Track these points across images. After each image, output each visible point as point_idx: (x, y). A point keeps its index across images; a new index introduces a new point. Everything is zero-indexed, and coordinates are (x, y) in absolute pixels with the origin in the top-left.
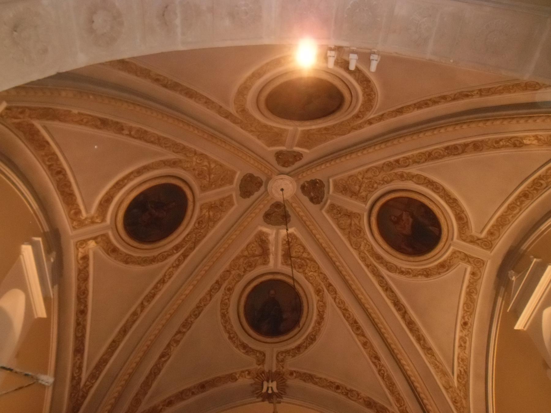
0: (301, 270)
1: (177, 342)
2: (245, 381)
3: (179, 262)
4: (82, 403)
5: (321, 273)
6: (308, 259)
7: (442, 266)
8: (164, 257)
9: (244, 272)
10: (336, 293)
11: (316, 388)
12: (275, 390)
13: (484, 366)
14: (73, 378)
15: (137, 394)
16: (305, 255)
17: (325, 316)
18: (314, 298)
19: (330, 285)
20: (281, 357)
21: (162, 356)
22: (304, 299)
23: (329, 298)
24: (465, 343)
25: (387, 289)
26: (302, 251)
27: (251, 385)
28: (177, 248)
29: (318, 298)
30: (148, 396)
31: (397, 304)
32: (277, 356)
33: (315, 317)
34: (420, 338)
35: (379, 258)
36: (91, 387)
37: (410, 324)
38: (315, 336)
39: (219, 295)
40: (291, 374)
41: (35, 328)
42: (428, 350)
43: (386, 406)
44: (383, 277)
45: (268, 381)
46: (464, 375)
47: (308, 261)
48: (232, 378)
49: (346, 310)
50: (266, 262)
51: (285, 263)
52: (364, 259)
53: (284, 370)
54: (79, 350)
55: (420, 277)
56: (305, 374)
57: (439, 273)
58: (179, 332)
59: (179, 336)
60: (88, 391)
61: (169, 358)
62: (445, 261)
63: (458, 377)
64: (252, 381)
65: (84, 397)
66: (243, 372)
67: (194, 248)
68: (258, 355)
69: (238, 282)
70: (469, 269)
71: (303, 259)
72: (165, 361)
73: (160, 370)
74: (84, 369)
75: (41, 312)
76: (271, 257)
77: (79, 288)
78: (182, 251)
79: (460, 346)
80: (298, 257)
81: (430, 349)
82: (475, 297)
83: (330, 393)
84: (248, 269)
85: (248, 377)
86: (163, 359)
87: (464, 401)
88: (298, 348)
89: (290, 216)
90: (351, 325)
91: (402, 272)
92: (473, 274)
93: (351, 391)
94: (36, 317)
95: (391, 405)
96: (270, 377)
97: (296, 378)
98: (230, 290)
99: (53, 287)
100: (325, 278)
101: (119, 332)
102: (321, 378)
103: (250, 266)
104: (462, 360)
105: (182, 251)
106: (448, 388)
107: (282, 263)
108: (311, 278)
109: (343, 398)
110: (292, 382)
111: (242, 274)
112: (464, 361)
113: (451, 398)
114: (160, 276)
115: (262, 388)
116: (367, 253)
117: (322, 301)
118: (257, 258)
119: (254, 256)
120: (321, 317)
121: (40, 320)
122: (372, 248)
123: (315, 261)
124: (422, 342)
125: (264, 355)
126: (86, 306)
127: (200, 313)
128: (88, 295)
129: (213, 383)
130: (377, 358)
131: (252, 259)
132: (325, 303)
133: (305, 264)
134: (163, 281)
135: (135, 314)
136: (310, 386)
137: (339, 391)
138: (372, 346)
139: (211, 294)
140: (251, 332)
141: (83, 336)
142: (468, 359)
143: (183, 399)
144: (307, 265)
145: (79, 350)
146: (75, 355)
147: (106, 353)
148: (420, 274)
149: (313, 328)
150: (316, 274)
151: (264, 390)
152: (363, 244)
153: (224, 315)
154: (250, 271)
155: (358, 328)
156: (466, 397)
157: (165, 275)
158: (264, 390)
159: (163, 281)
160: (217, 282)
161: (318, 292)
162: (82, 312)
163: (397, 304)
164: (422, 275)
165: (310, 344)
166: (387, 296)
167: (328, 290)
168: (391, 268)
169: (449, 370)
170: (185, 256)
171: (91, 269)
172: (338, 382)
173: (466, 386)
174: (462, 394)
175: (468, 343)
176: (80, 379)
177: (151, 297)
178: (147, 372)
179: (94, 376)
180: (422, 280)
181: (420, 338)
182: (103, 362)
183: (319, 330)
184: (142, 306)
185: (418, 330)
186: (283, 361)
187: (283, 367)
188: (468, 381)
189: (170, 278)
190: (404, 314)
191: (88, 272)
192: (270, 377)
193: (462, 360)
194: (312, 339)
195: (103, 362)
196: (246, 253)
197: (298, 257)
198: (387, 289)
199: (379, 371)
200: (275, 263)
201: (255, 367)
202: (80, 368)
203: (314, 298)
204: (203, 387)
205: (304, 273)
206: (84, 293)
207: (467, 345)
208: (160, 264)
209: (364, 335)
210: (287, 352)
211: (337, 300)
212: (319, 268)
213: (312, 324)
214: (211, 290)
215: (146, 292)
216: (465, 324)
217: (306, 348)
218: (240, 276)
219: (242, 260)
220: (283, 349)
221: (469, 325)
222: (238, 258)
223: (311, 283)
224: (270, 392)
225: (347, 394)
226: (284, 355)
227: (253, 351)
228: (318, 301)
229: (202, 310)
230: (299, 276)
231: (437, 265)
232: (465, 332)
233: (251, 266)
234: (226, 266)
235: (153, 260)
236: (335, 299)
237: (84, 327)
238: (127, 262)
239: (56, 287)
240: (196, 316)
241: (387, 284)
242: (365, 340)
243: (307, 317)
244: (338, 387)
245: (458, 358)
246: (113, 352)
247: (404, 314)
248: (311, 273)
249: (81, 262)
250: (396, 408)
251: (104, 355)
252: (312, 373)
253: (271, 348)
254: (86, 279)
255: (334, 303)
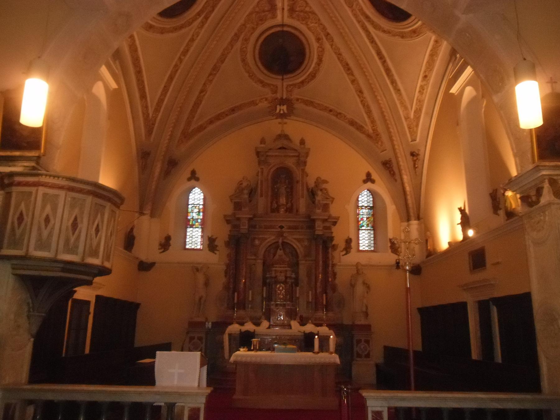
0: (304, 22)
1: (211, 81)
2: (264, 105)
3: (203, 23)
4: (153, 128)
5: (321, 24)
6: (310, 12)
7: (414, 31)
8: (190, 23)
9: (257, 25)
10: (333, 41)
11: (316, 110)
12: (286, 111)
13: (432, 109)
14: (143, 114)
15: (188, 118)
16: (307, 9)
17: (323, 59)
18: (315, 45)
19: (328, 34)
20: (290, 89)
21: (202, 91)
22: (307, 46)
23: (327, 46)
24: (423, 90)
25: (372, 41)
26: (305, 5)
27: (269, 107)
28: (199, 14)
29: (318, 45)
30: (195, 119)
31: (379, 53)
32: (287, 88)
33: (315, 60)
34: (393, 82)
35: (367, 17)
36: (157, 117)
37: (388, 71)
38: (315, 74)
39: (238, 45)
40: (298, 100)
41: (113, 95)
42: (398, 90)
43: (363, 125)
44: (370, 33)
45: (280, 105)
46: (418, 112)
47: (310, 14)
48: (253, 103)
49: (340, 54)
50: (274, 16)
51: (291, 16)
52: (355, 15)
53: (292, 97)
54: (143, 96)
55: (397, 37)
56: (307, 100)
57: (411, 37)
58: (210, 74)
59: (211, 78)
60: (155, 120)
61: (206, 93)
62: (416, 29)
63: (415, 112)
64: (269, 105)
65: (154, 124)
66: (262, 99)
67: (213, 10)
68: (272, 87)
69: (252, 33)
70: (434, 38)
71: (306, 12)
72: (204, 95)
73: (201, 101)
74: (150, 108)
75: (113, 85)
76: (279, 13)
77: (132, 57)
78: (203, 16)
79: (420, 92)
80: (302, 11)
81: (399, 90)
82: (436, 58)
83: (326, 114)
84: (260, 22)
85: (266, 102)
86: (202, 94)
87: (415, 129)
88: (302, 82)
89: (209, 250)
90: (343, 66)
91: (384, 31)
92: (436, 41)
93: (340, 113)
94: (112, 89)
95: (366, 125)
96: (282, 102)
97: (300, 103)
98: (246, 40)
99: (115, 63)
100: (324, 29)
101: (168, 80)
102: (319, 104)
103: (261, 20)
104: (420, 101)
105: (203, 16)
106: (407, 118)
107: (288, 17)
108: (312, 29)
109: (334, 118)
110: (299, 106)
111: (255, 26)
112: (420, 102)
113: (408, 125)
114: (190, 37)
115: (276, 109)
116: (358, 11)
117: (321, 47)
118: (267, 13)
119: (264, 11)
120: (320, 60)
121: (115, 90)
122: (362, 9)
123: (316, 14)
124: (394, 84)
125: (277, 87)
126: (140, 68)
127: (225, 59)
128: (139, 61)
129: (239, 108)
130: (361, 92)
131: (263, 14)
132: (323, 49)
133: (308, 17)
134: (192, 40)
135: (176, 66)
136: (310, 109)
137: (332, 113)
138: (358, 84)
139: (232, 44)
140: (265, 71)
141: (144, 87)
142: (423, 101)
143: (220, 119)
144: (309, 18)
145: (143, 96)
146: (141, 100)
147: (162, 95)
148: (397, 35)
149: (314, 68)
150: (316, 25)
151: (278, 111)
152: (355, 4)
153: (243, 60)
154: (262, 24)
155: (349, 69)
156: (417, 126)
157: (193, 35)
158: (278, 111)
159: (192, 40)
160: (236, 34)
161: (318, 40)
162: (139, 72)
163: (379, 53)
164: (399, 36)
165: (311, 80)
166: (372, 47)
167: (327, 39)
168: (376, 27)
169: (409, 107)
170: (206, 18)
171: (137, 42)
172: (332, 107)
173: (418, 118)
174: (415, 124)
175: (425, 90)
176: (149, 114)
177: (185, 52)
178: (192, 104)
179: (157, 110)
180: (398, 40)
181: (393, 82)
182: (161, 101)
183: (319, 69)
184: (180, 60)
185: (392, 75)
186: (291, 91)
187: (291, 95)
188: (420, 116)
189: (197, 36)
190: (384, 62)
191: (136, 46)
192: (282, 102)
193: (420, 101)
194: (313, 76)
195: (161, 101)
196: (257, 9)
197: (302, 11)
198: (372, 41)
199: (362, 101)
200: (282, 17)
201: (270, 95)
202: (147, 107)
203: (315, 45)
204: (233, 110)
205: (307, 24)
206: (137, 59)
207: (425, 91)
208: (187, 29)
209: (352, 75)
210: (294, 85)
211: (334, 47)
212: (319, 20)
213: (313, 65)
214: (231, 41)
215: (182, 49)
216: (425, 77)
217: (308, 82)
218: (254, 29)
219: (254, 15)
220: (291, 83)
221: (428, 78)
222: (251, 14)
223: (313, 33)
224: (282, 112)
225: (337, 116)
226: (292, 87)
227: (269, 85)
228: (319, 47)
229: (226, 57)
230: (303, 28)
231: (411, 31)
232: (424, 83)
233: (262, 20)
234: (242, 21)
235: (181, 27)
236: (332, 45)
237: (143, 82)
238: (162, 33)
239: (117, 62)
240: (223, 62)
241: (373, 38)
242: (353, 78)
243: (302, 71)
244: (331, 111)
245: (417, 100)
246: (166, 93)
247: (384, 62)
248: (312, 24)
249: (129, 40)
250: (370, 127)
251: (160, 96)
252: (312, 100)
253: (282, 84)
254: (136, 50)
255: (331, 49)
